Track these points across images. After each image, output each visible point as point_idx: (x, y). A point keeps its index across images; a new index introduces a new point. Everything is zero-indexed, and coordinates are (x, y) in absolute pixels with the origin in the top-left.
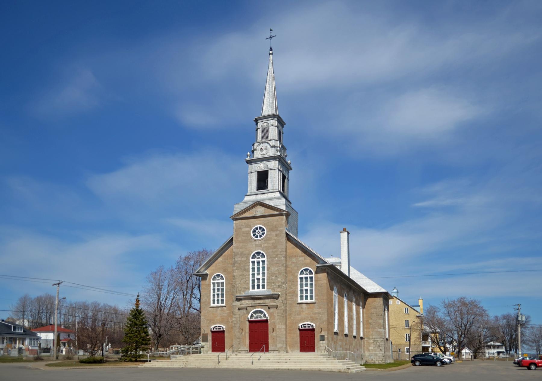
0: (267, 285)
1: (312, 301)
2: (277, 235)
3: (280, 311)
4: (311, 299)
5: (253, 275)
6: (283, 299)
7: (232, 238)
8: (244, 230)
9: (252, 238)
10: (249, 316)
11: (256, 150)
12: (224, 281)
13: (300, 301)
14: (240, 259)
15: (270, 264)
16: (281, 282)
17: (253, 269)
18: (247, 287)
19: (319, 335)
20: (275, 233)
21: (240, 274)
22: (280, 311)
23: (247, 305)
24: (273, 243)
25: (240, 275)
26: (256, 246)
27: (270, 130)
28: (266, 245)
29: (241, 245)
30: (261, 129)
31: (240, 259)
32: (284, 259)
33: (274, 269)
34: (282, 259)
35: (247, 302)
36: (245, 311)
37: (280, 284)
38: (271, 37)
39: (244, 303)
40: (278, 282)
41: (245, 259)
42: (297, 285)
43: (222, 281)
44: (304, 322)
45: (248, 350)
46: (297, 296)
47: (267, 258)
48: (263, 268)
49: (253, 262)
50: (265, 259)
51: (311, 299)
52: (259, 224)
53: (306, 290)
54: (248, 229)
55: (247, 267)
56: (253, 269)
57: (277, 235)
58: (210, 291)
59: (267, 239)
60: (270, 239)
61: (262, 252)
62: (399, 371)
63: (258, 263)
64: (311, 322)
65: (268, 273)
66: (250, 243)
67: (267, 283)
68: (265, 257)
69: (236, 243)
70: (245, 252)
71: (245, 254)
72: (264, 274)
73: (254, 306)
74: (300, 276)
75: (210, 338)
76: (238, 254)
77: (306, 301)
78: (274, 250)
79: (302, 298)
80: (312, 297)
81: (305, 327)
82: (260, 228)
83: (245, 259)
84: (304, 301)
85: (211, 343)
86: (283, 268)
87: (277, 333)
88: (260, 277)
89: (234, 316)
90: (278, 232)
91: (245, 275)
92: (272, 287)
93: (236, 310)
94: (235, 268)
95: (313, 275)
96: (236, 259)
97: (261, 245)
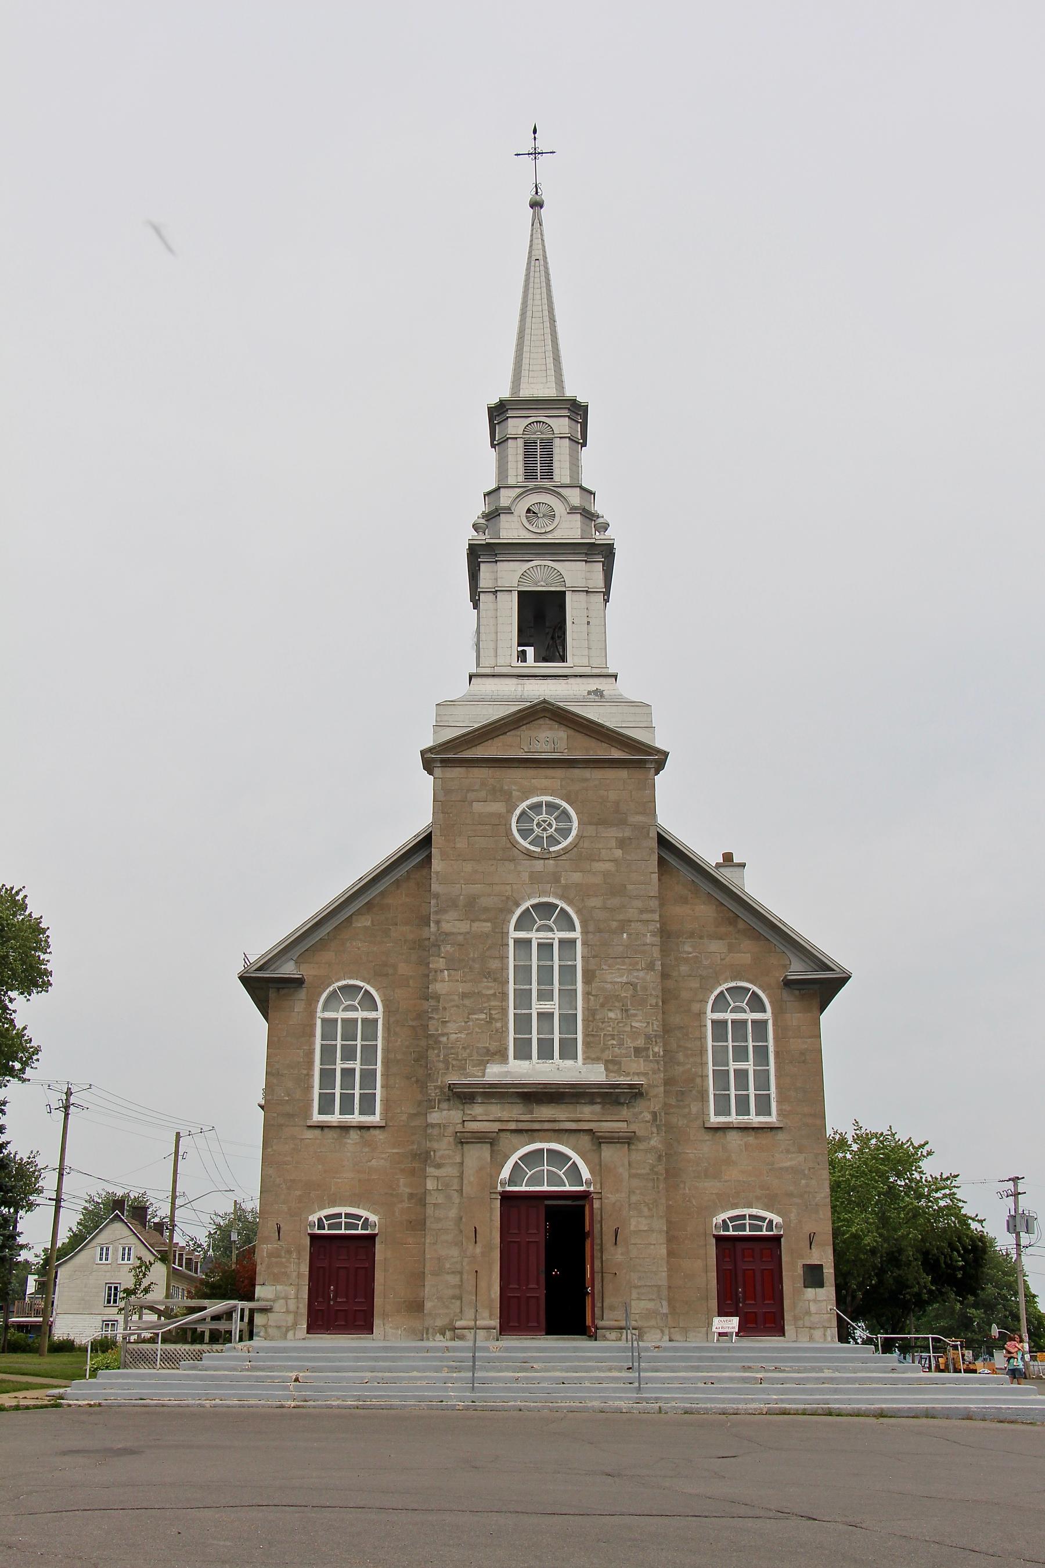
0: (587, 1044)
1: (762, 1119)
3: (643, 1157)
5: (523, 998)
6: (656, 1105)
8: (477, 807)
9: (514, 844)
10: (505, 1173)
11: (508, 511)
12: (379, 1014)
13: (714, 1120)
14: (463, 927)
16: (648, 1037)
17: (523, 972)
18: (493, 1046)
19: (800, 1263)
20: (613, 833)
21: (461, 988)
22: (643, 1157)
23: (496, 1127)
24: (606, 874)
25: (464, 996)
26: (535, 878)
27: (556, 450)
28: (577, 877)
29: (468, 867)
30: (520, 443)
31: (463, 927)
32: (657, 940)
33: (615, 977)
34: (649, 939)
35: (496, 1110)
36: (485, 1151)
37: (640, 1042)
38: (535, 153)
39: (484, 1116)
40: (635, 1034)
41: (487, 927)
42: (703, 1051)
43: (372, 1015)
44: (735, 1206)
45: (496, 1323)
46: (703, 1096)
47: (585, 932)
48: (567, 972)
49: (523, 944)
52: (544, 791)
54: (497, 807)
55: (494, 965)
56: (523, 972)
58: (311, 1052)
60: (594, 857)
61: (562, 904)
63: (545, 948)
64: (767, 1208)
65: (587, 994)
66: (511, 866)
67: (586, 1035)
69: (444, 856)
70: (485, 902)
71: (486, 909)
73: (531, 1134)
74: (711, 1016)
76: (454, 904)
77: (743, 1119)
78: (615, 902)
79: (723, 1108)
81: (742, 1227)
82: (552, 807)
83: (487, 927)
84: (734, 1118)
86: (651, 979)
87: (639, 1258)
88: (553, 1006)
89: (430, 1170)
91: (489, 998)
92: (608, 1055)
93: (443, 1147)
94: (441, 963)
96: (446, 927)
97: (556, 878)
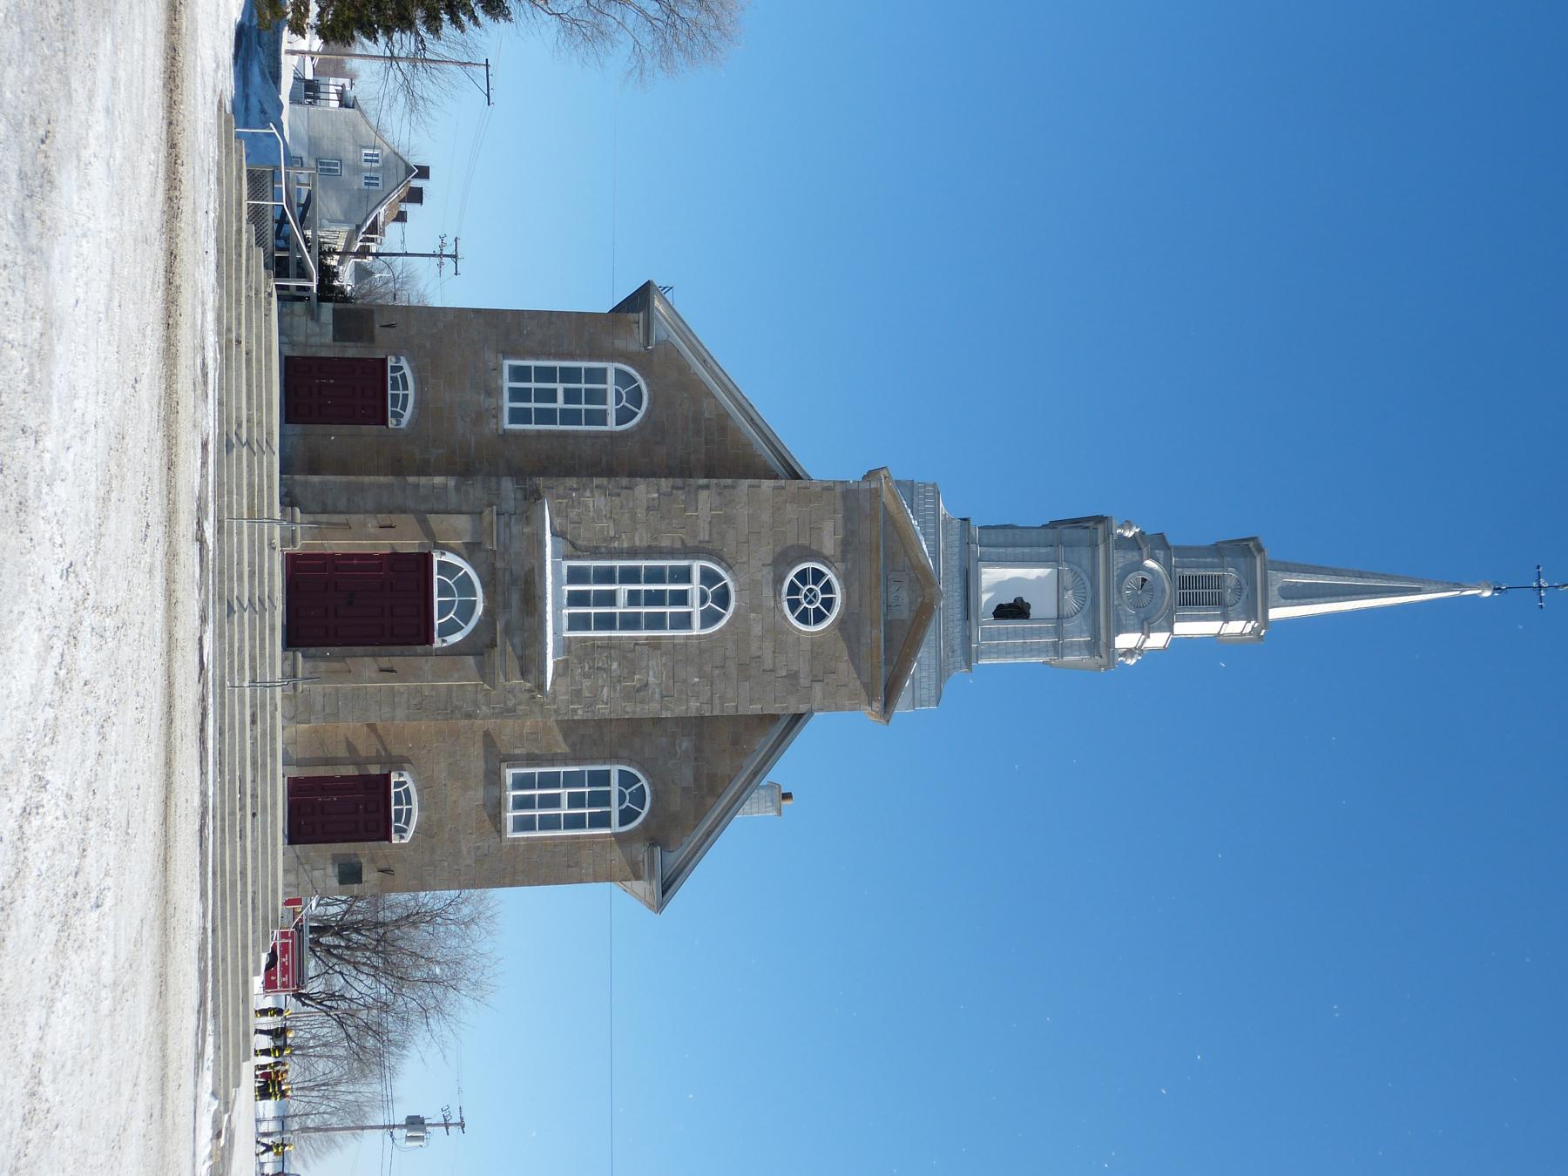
1: (510, 825)
2: (793, 676)
4: (512, 410)
5: (630, 576)
7: (799, 478)
10: (450, 558)
15: (674, 646)
20: (803, 667)
28: (757, 630)
29: (766, 517)
34: (694, 704)
45: (298, 549)
47: (699, 637)
50: (696, 630)
51: (512, 410)
53: (554, 801)
57: (793, 676)
58: (572, 357)
59: (778, 631)
62: (211, 376)
68: (704, 626)
72: (630, 622)
74: (615, 770)
75: (352, 351)
78: (732, 669)
80: (525, 824)
85: (325, 353)
87: (370, 697)
88: (621, 608)
90: (804, 682)
95: (616, 827)
